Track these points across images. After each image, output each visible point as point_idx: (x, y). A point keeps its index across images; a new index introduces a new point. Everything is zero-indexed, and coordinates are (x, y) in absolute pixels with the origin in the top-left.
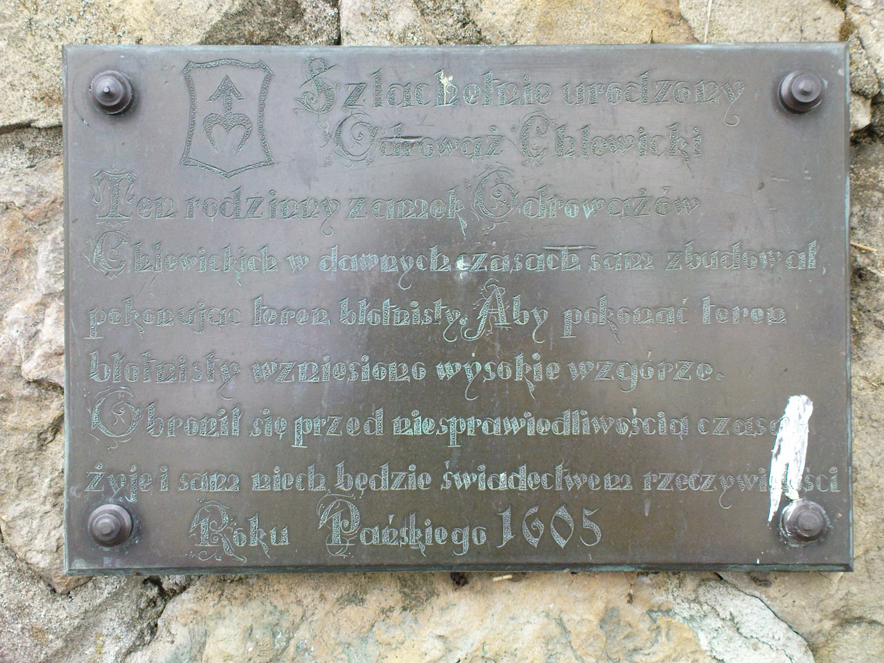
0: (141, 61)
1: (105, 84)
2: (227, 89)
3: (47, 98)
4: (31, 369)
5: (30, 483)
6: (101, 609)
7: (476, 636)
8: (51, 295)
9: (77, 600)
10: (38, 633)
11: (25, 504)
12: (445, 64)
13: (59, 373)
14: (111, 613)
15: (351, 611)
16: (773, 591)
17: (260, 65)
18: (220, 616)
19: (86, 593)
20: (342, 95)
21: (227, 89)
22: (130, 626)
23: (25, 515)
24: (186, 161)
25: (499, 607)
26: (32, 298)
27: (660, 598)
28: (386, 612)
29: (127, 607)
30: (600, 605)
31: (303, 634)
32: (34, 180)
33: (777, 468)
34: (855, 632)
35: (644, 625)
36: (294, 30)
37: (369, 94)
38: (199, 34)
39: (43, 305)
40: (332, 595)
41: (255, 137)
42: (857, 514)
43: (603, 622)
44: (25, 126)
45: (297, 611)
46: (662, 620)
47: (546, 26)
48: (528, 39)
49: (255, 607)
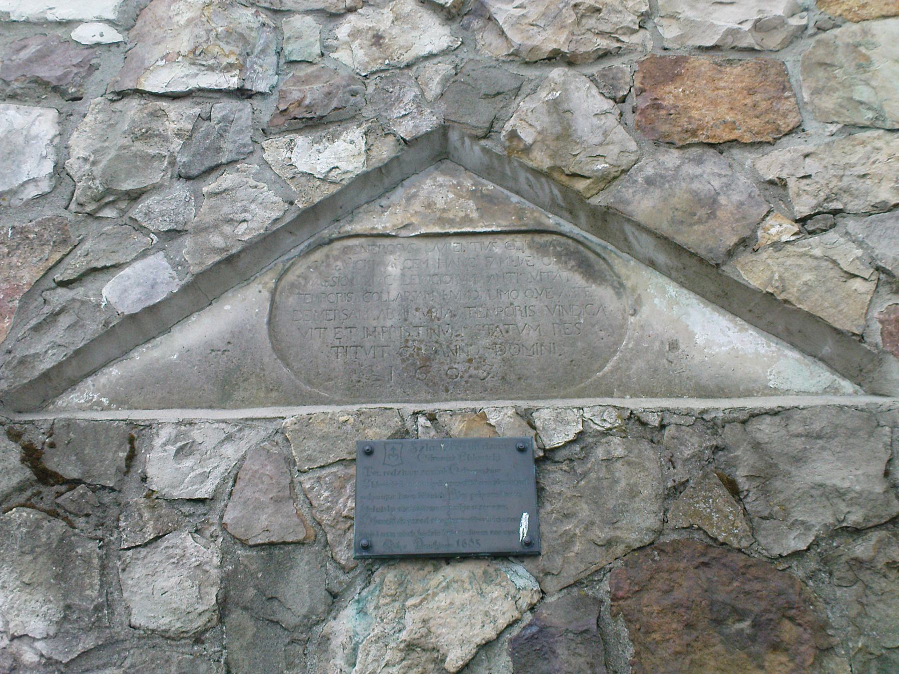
0: (374, 443)
1: (367, 448)
2: (393, 449)
3: (350, 453)
4: (345, 513)
5: (341, 543)
6: (356, 577)
7: (452, 576)
8: (350, 496)
9: (351, 574)
10: (340, 583)
11: (340, 548)
12: (442, 442)
13: (352, 514)
14: (359, 578)
15: (421, 572)
16: (525, 563)
17: (401, 443)
18: (388, 573)
19: (353, 572)
20: (419, 449)
21: (393, 449)
22: (363, 582)
23: (341, 550)
24: (384, 464)
25: (458, 569)
26: (345, 497)
27: (498, 566)
28: (429, 572)
29: (363, 576)
30: (483, 569)
31: (409, 577)
32: (347, 471)
33: (521, 530)
34: (549, 578)
35: (494, 574)
36: (407, 437)
37: (425, 448)
38: (386, 438)
39: (348, 499)
40: (416, 568)
41: (399, 459)
42: (543, 542)
43: (484, 573)
44: (344, 460)
45: (407, 572)
46: (498, 572)
47: (466, 434)
48: (462, 436)
49: (397, 570)
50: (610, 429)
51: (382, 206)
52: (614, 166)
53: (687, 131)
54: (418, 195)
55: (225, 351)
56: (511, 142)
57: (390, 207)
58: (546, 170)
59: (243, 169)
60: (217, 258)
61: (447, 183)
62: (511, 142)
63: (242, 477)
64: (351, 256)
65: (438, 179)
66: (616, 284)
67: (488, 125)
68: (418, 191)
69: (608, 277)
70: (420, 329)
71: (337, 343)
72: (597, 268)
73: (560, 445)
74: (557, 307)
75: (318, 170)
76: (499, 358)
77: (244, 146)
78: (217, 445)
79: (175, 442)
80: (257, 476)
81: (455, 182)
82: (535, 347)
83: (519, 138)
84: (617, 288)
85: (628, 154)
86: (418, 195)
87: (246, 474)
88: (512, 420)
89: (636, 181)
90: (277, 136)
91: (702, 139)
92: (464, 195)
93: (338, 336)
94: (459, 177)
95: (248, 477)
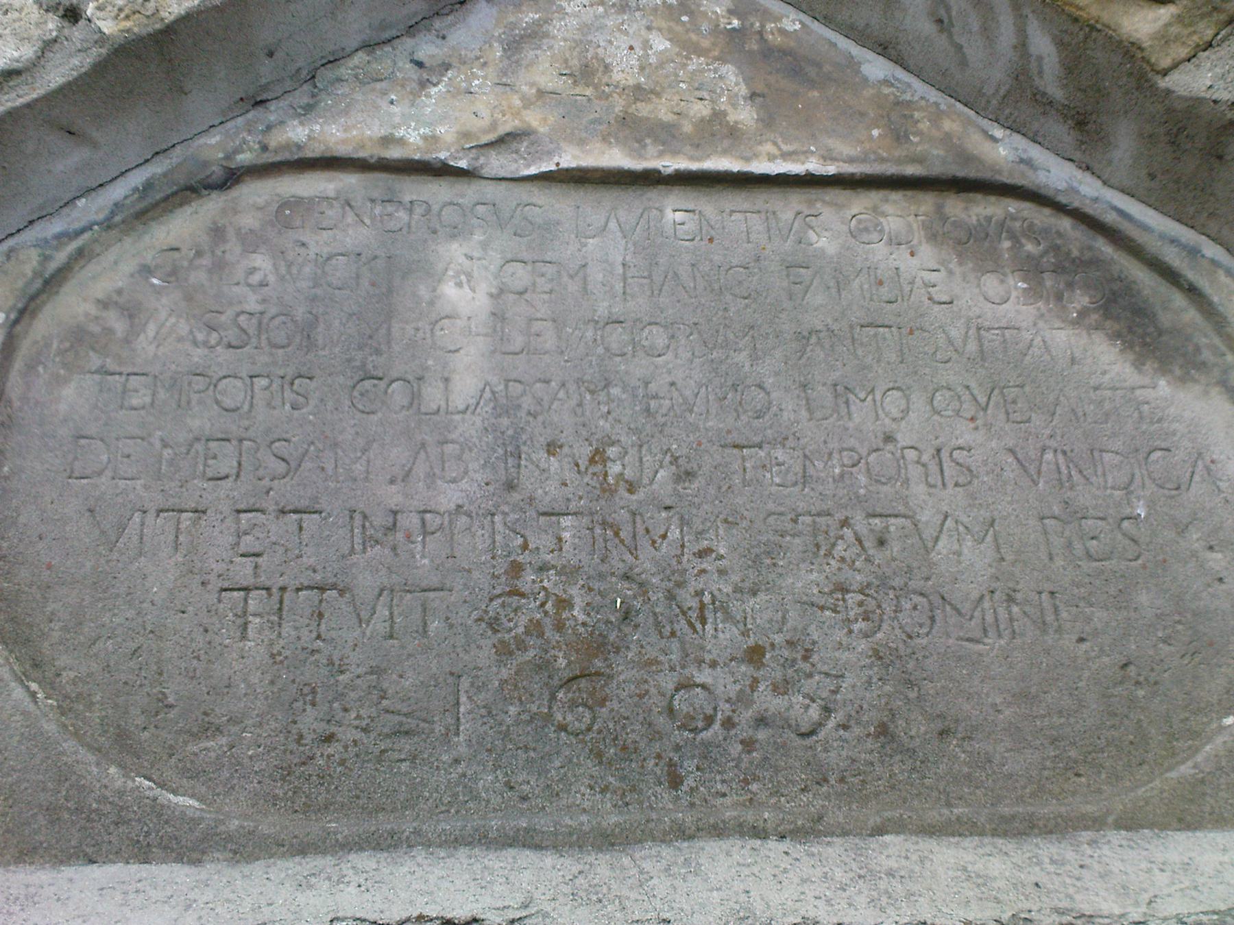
51: (420, 64)
54: (546, 35)
57: (447, 67)
68: (547, 21)
69: (1206, 355)
70: (566, 521)
72: (1165, 319)
86: (546, 35)
92: (706, 43)
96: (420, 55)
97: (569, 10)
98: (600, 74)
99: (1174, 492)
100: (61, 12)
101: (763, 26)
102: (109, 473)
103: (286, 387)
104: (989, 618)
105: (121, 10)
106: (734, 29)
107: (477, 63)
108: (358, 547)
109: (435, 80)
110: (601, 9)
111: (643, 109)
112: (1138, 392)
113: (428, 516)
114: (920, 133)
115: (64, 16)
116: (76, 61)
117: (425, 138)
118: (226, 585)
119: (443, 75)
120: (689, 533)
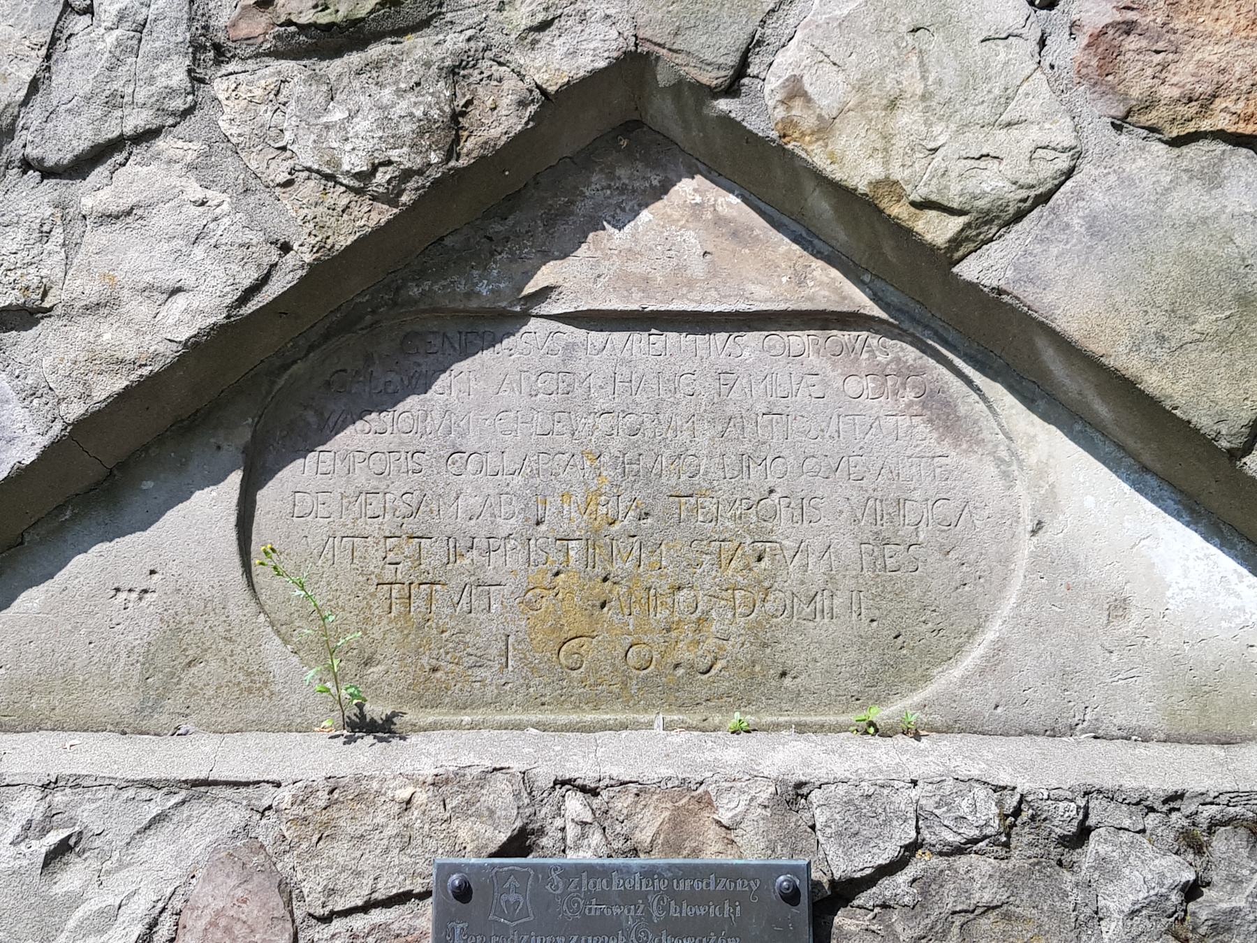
50: (975, 841)
51: (490, 239)
52: (1021, 187)
53: (1190, 100)
54: (572, 213)
55: (145, 591)
56: (789, 108)
57: (507, 239)
58: (867, 190)
59: (171, 152)
60: (119, 384)
61: (637, 184)
62: (789, 108)
63: (190, 924)
64: (420, 360)
65: (618, 173)
66: (1004, 454)
67: (733, 60)
68: (572, 202)
69: (985, 435)
70: (572, 544)
71: (388, 575)
72: (962, 410)
73: (868, 871)
74: (871, 503)
75: (346, 167)
76: (741, 621)
77: (171, 92)
78: (133, 838)
79: (44, 832)
80: (223, 922)
81: (655, 183)
82: (818, 598)
83: (808, 99)
84: (1003, 461)
85: (1051, 154)
86: (572, 213)
87: (199, 917)
88: (768, 813)
89: (1068, 225)
90: (251, 65)
91: (1221, 122)
92: (676, 215)
93: (391, 557)
94: (665, 170)
95: (202, 924)
96: (490, 232)
97: (587, 194)
98: (605, 241)
99: (946, 528)
100: (279, 245)
101: (715, 201)
102: (313, 514)
103: (409, 459)
104: (819, 606)
105: (313, 247)
106: (696, 204)
107: (527, 237)
108: (452, 559)
109: (499, 249)
110: (609, 192)
111: (632, 267)
112: (936, 459)
113: (491, 540)
114: (813, 279)
115: (280, 248)
116: (289, 277)
117: (492, 291)
118: (381, 581)
119: (505, 246)
120: (635, 510)
